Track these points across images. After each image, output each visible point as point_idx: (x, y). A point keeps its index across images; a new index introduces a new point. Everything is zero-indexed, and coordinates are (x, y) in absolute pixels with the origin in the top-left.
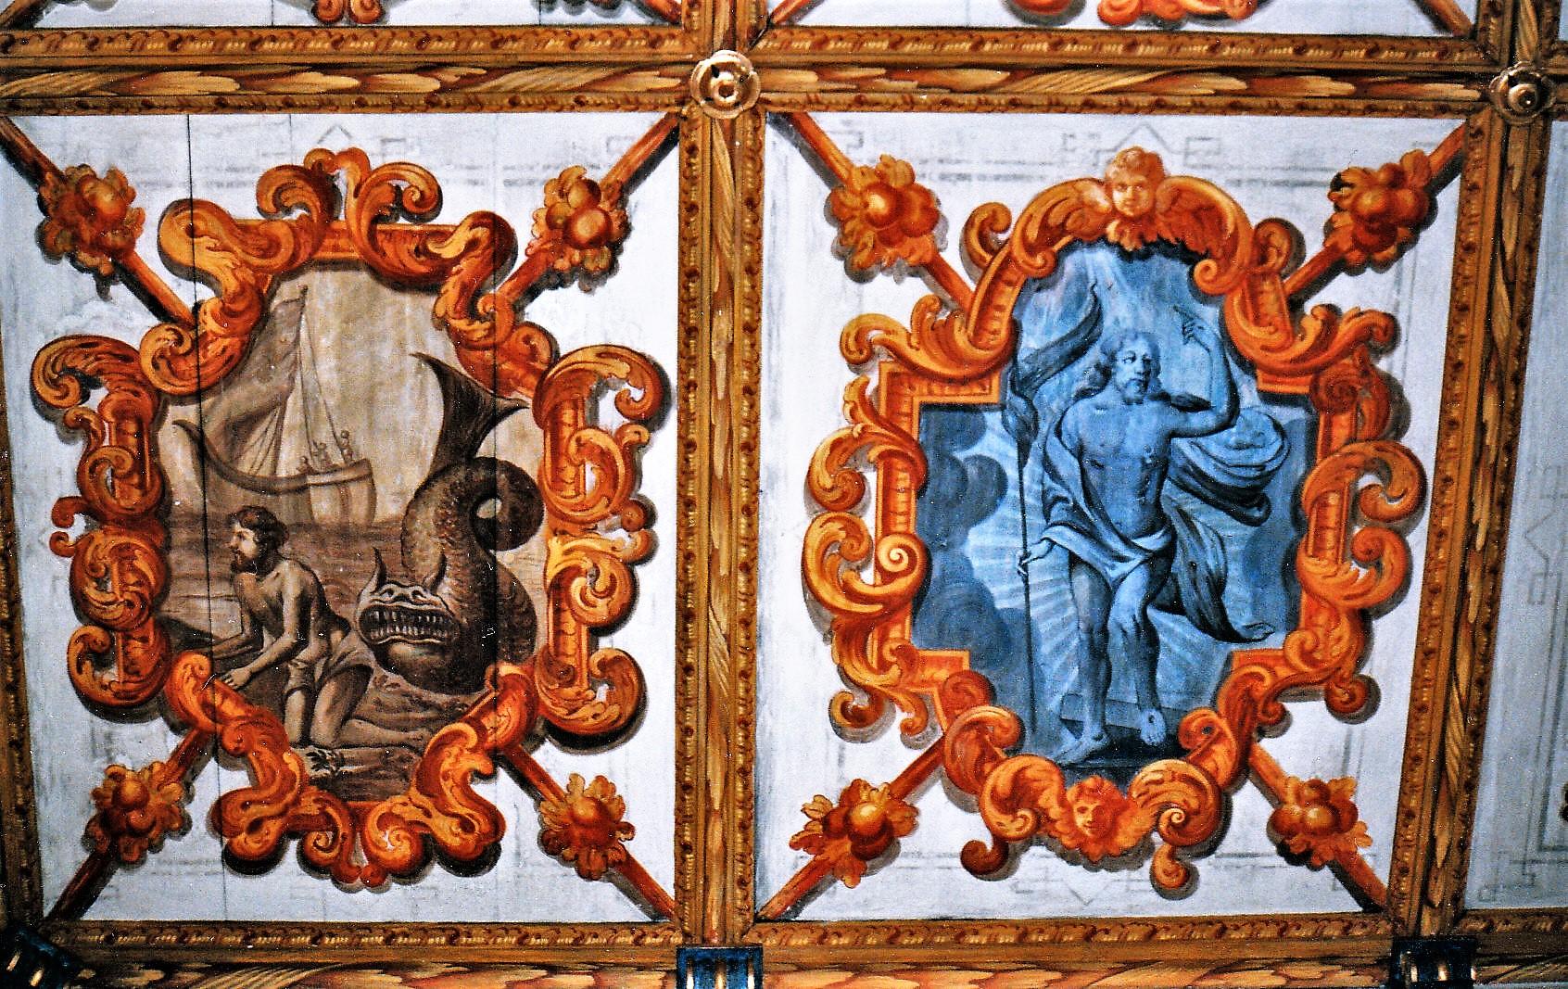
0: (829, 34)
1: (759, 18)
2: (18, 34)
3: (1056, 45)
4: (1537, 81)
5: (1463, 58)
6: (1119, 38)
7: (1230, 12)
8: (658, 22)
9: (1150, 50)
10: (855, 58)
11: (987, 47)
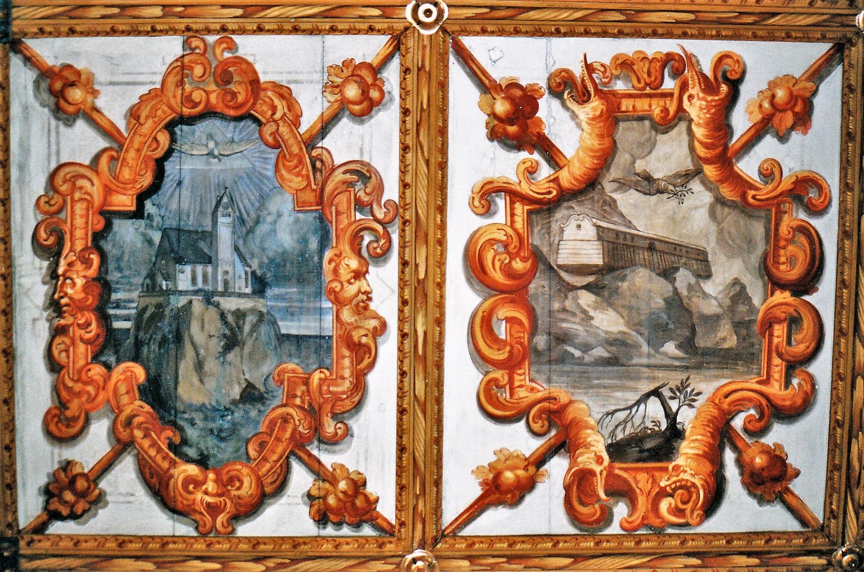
0: (476, 540)
1: (437, 531)
2: (36, 537)
3: (597, 544)
4: (858, 553)
5: (818, 542)
6: (632, 538)
7: (690, 521)
8: (383, 534)
9: (650, 544)
10: (490, 553)
11: (561, 545)
